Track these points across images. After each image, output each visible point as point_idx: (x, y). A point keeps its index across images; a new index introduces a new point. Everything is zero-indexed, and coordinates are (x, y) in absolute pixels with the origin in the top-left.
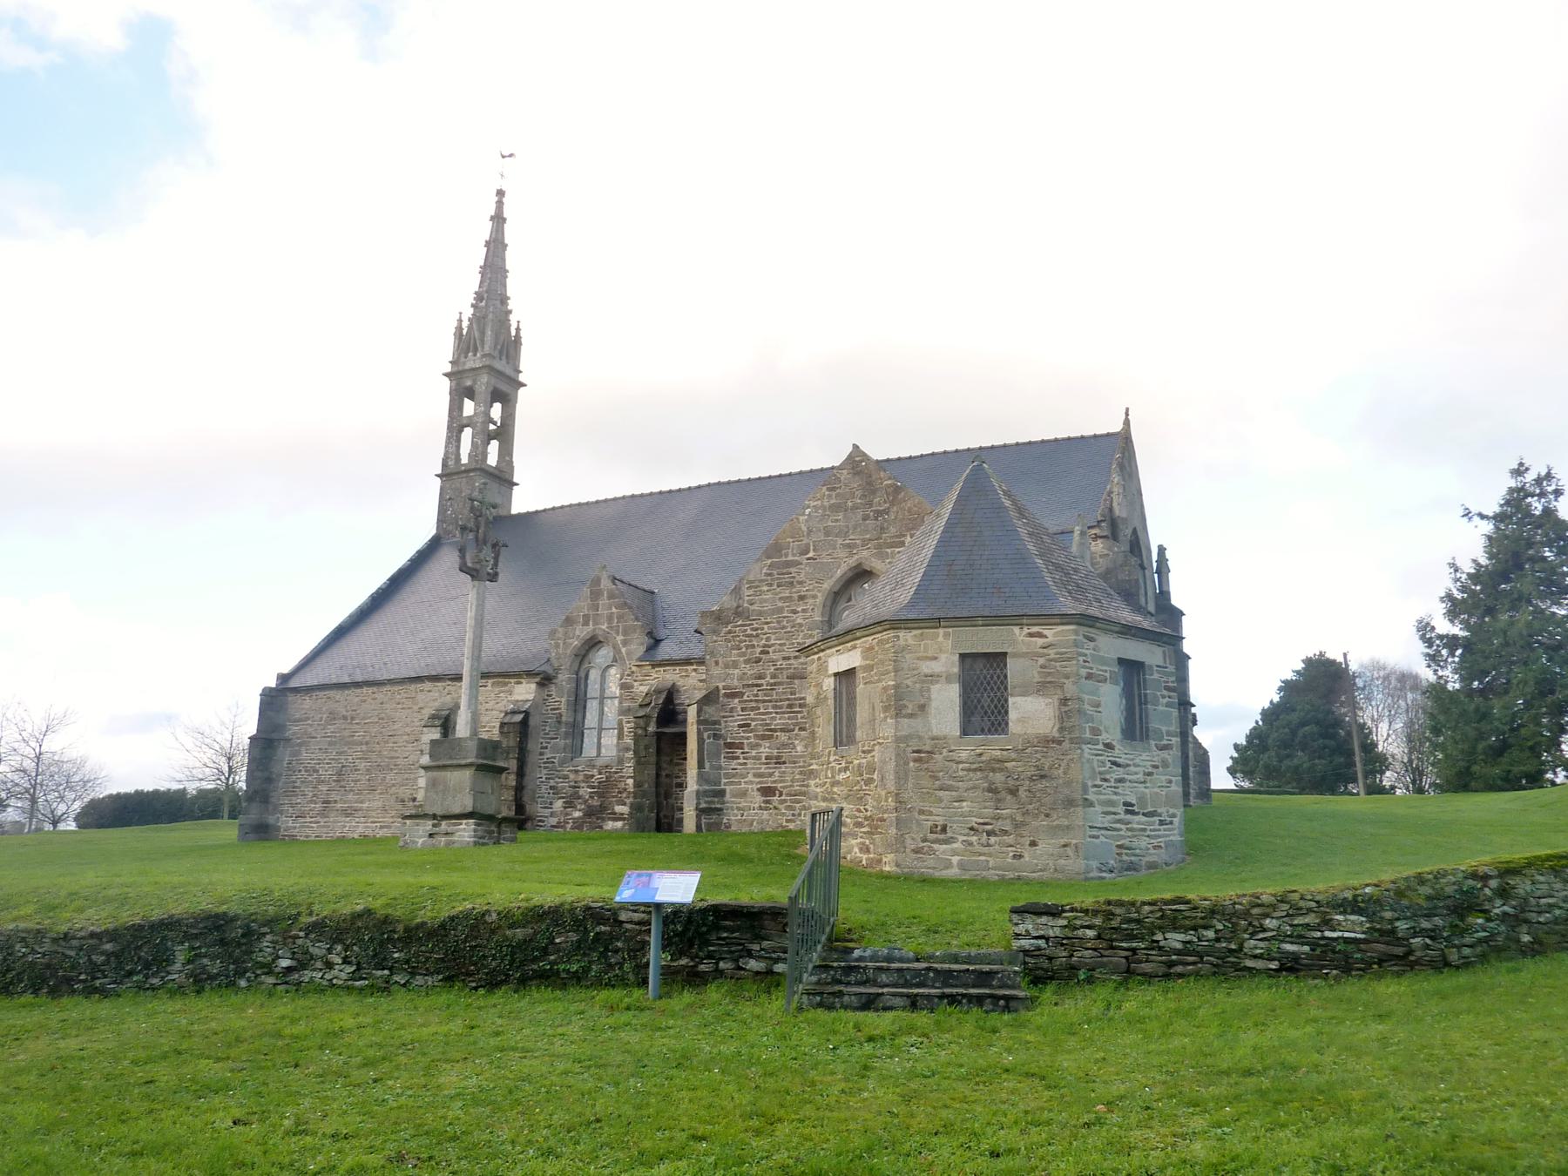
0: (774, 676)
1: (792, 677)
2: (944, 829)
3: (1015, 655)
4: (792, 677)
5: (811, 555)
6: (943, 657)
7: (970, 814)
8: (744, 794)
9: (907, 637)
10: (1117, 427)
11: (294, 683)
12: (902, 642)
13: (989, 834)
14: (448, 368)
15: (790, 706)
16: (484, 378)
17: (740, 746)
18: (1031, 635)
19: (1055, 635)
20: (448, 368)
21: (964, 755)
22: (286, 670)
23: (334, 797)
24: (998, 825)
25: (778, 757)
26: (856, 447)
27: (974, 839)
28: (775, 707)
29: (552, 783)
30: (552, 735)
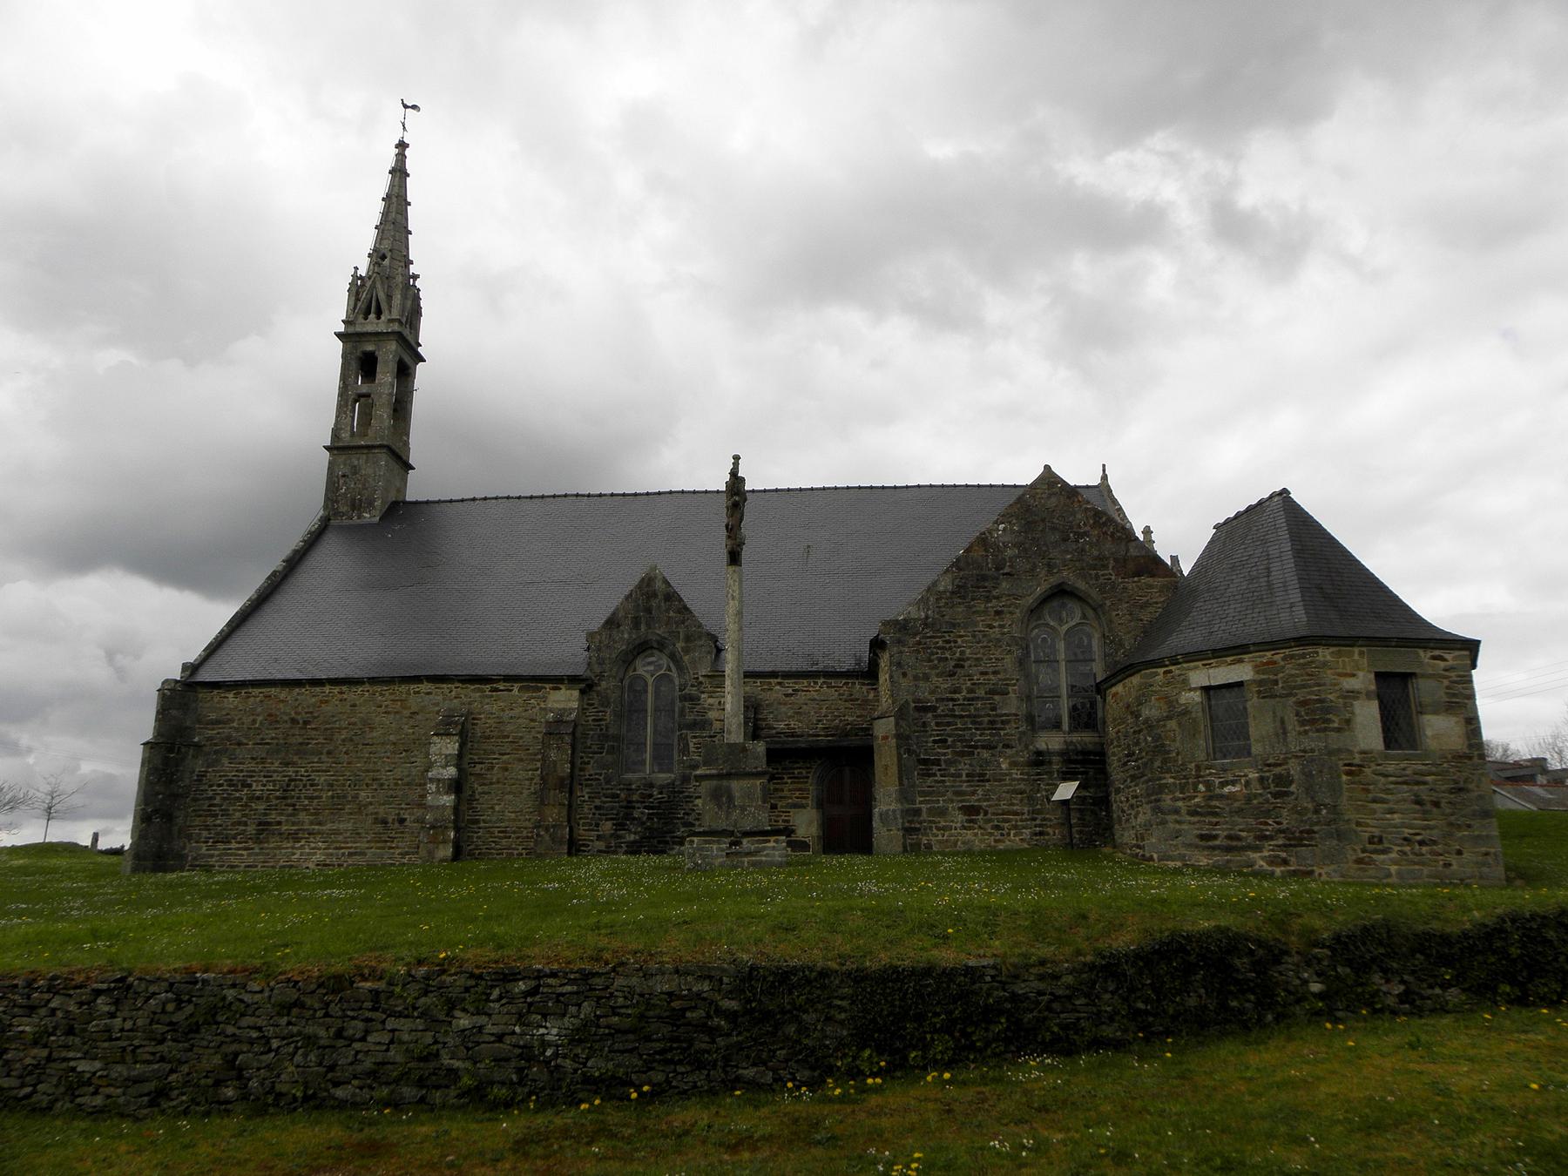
0: (971, 691)
1: (992, 692)
2: (1381, 841)
3: (1423, 676)
4: (992, 692)
5: (1007, 570)
6: (1361, 674)
7: (1404, 825)
8: (942, 813)
9: (1325, 654)
10: (1096, 481)
11: (205, 676)
12: (1320, 658)
13: (1421, 843)
14: (341, 328)
15: (991, 722)
16: (393, 346)
17: (937, 762)
18: (1434, 658)
19: (1455, 658)
20: (341, 328)
21: (1391, 769)
22: (192, 657)
23: (273, 817)
24: (1426, 835)
25: (981, 775)
26: (1047, 468)
27: (1407, 849)
28: (973, 723)
29: (598, 803)
30: (595, 748)
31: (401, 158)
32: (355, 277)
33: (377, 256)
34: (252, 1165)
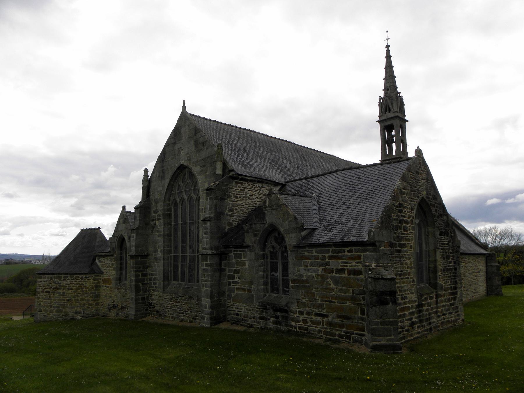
14: (378, 119)
20: (378, 119)
31: (388, 51)
32: (380, 99)
33: (386, 90)
34: (120, 307)
